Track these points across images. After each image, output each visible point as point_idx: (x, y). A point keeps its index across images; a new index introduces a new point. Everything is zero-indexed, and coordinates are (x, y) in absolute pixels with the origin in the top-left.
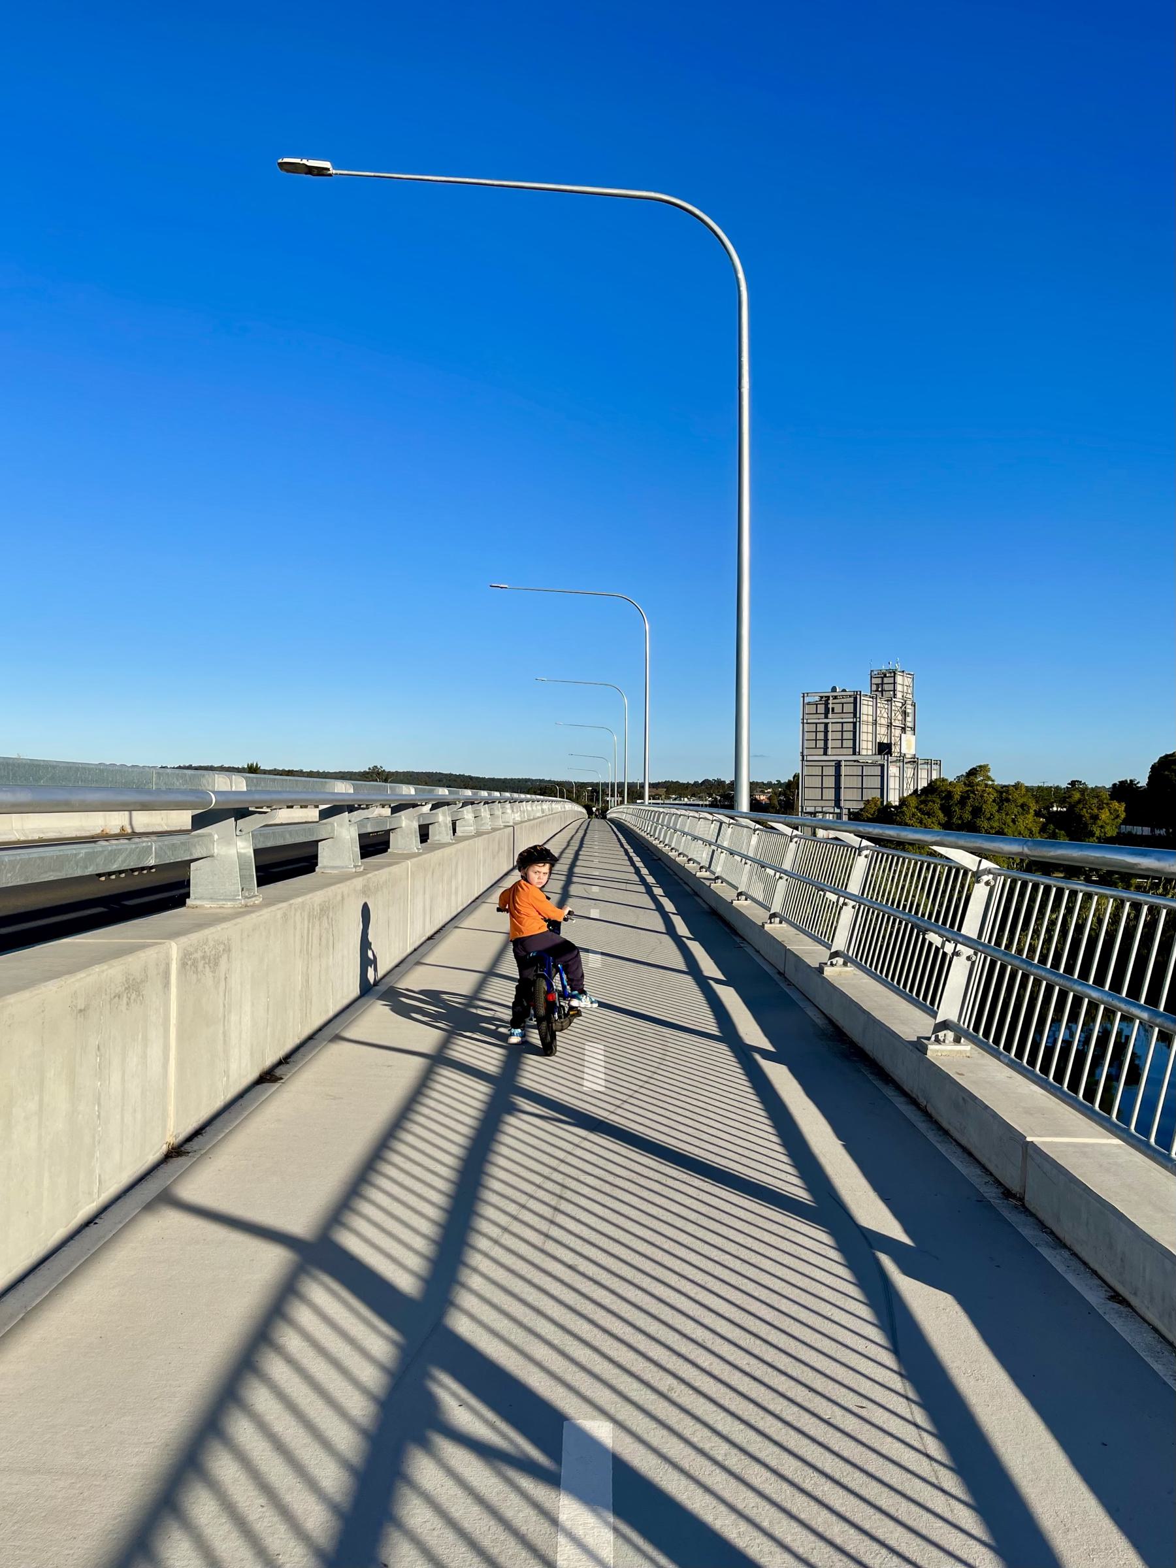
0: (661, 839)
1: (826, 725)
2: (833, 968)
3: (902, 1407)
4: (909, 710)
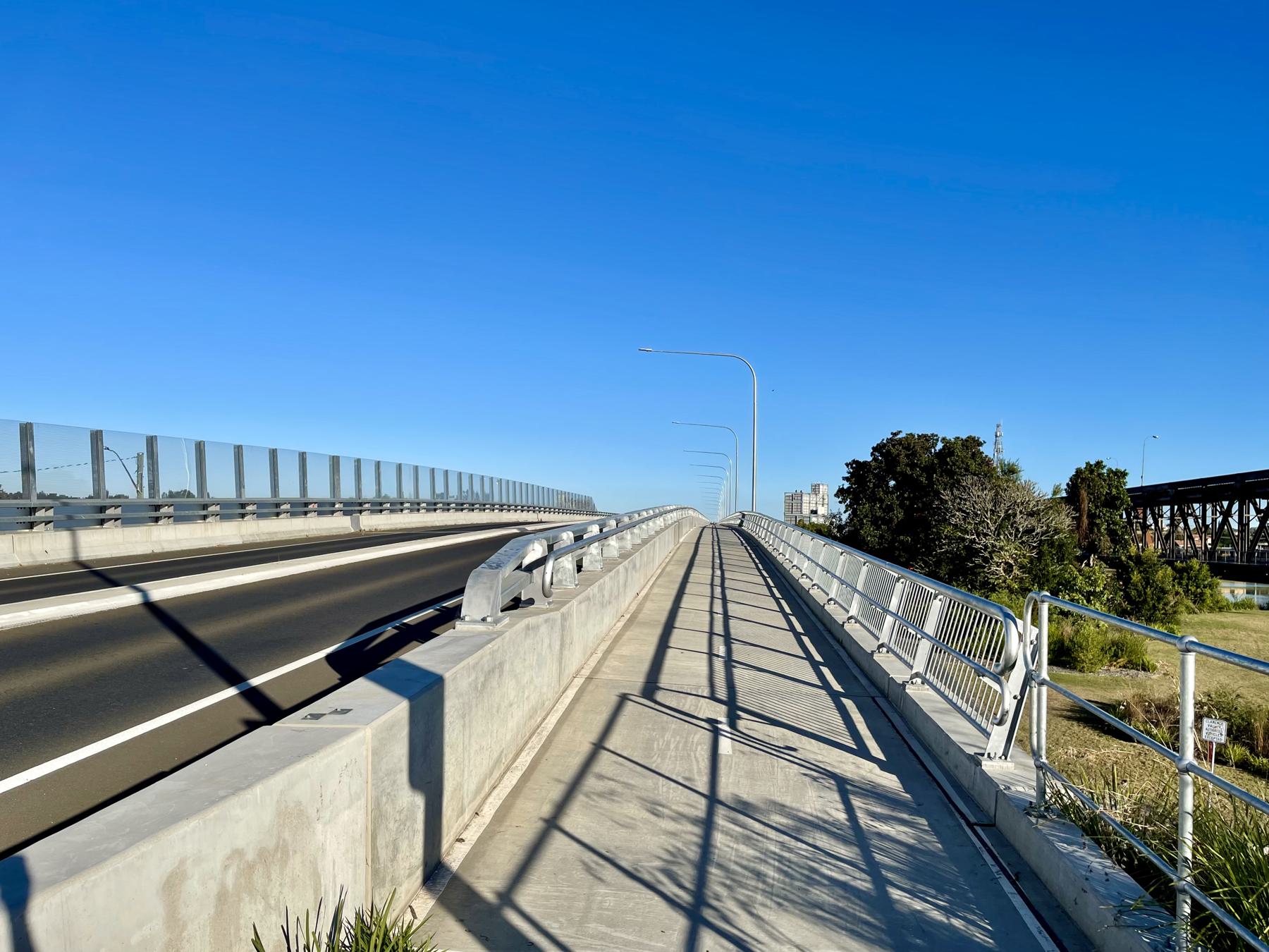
0: (771, 543)
4: (826, 497)
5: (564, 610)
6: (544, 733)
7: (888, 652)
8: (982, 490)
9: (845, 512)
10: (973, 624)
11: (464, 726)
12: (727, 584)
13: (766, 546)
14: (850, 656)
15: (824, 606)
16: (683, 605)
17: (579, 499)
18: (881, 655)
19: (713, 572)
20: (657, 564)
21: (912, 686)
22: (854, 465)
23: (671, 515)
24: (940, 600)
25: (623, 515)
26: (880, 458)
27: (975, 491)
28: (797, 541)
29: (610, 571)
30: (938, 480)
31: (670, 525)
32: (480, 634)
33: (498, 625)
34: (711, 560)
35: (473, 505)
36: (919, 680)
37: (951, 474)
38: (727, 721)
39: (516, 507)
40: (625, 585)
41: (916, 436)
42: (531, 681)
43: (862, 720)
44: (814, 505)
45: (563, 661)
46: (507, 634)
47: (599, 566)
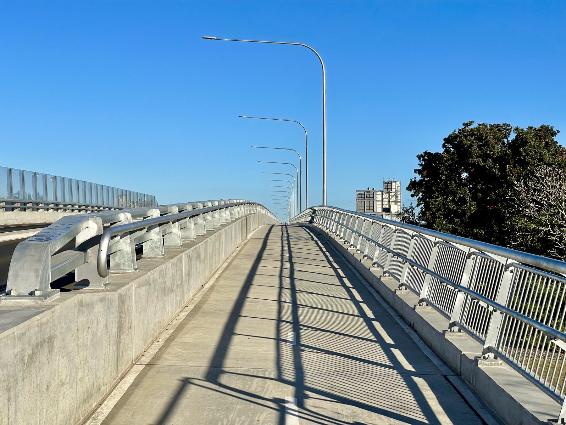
1: (365, 201)
2: (451, 333)
3: (422, 417)
4: (398, 195)
5: (122, 290)
6: (99, 417)
7: (460, 331)
8: (556, 180)
9: (417, 206)
10: (549, 317)
11: (9, 400)
12: (296, 275)
13: (337, 239)
14: (421, 338)
15: (395, 292)
16: (250, 295)
17: (140, 200)
18: (453, 334)
19: (282, 264)
20: (223, 257)
21: (484, 362)
22: (426, 158)
23: (239, 209)
24: (511, 272)
25: (186, 204)
26: (452, 149)
27: (549, 181)
28: (368, 231)
29: (172, 258)
30: (511, 171)
31: (236, 220)
32: (28, 308)
33: (48, 299)
34: (280, 253)
35: (25, 204)
36: (491, 355)
37: (524, 164)
38: (295, 400)
39: (73, 206)
40: (189, 274)
41: (488, 126)
42: (86, 361)
43: (433, 396)
44: (386, 203)
45: (121, 345)
46: (57, 307)
47: (160, 253)
